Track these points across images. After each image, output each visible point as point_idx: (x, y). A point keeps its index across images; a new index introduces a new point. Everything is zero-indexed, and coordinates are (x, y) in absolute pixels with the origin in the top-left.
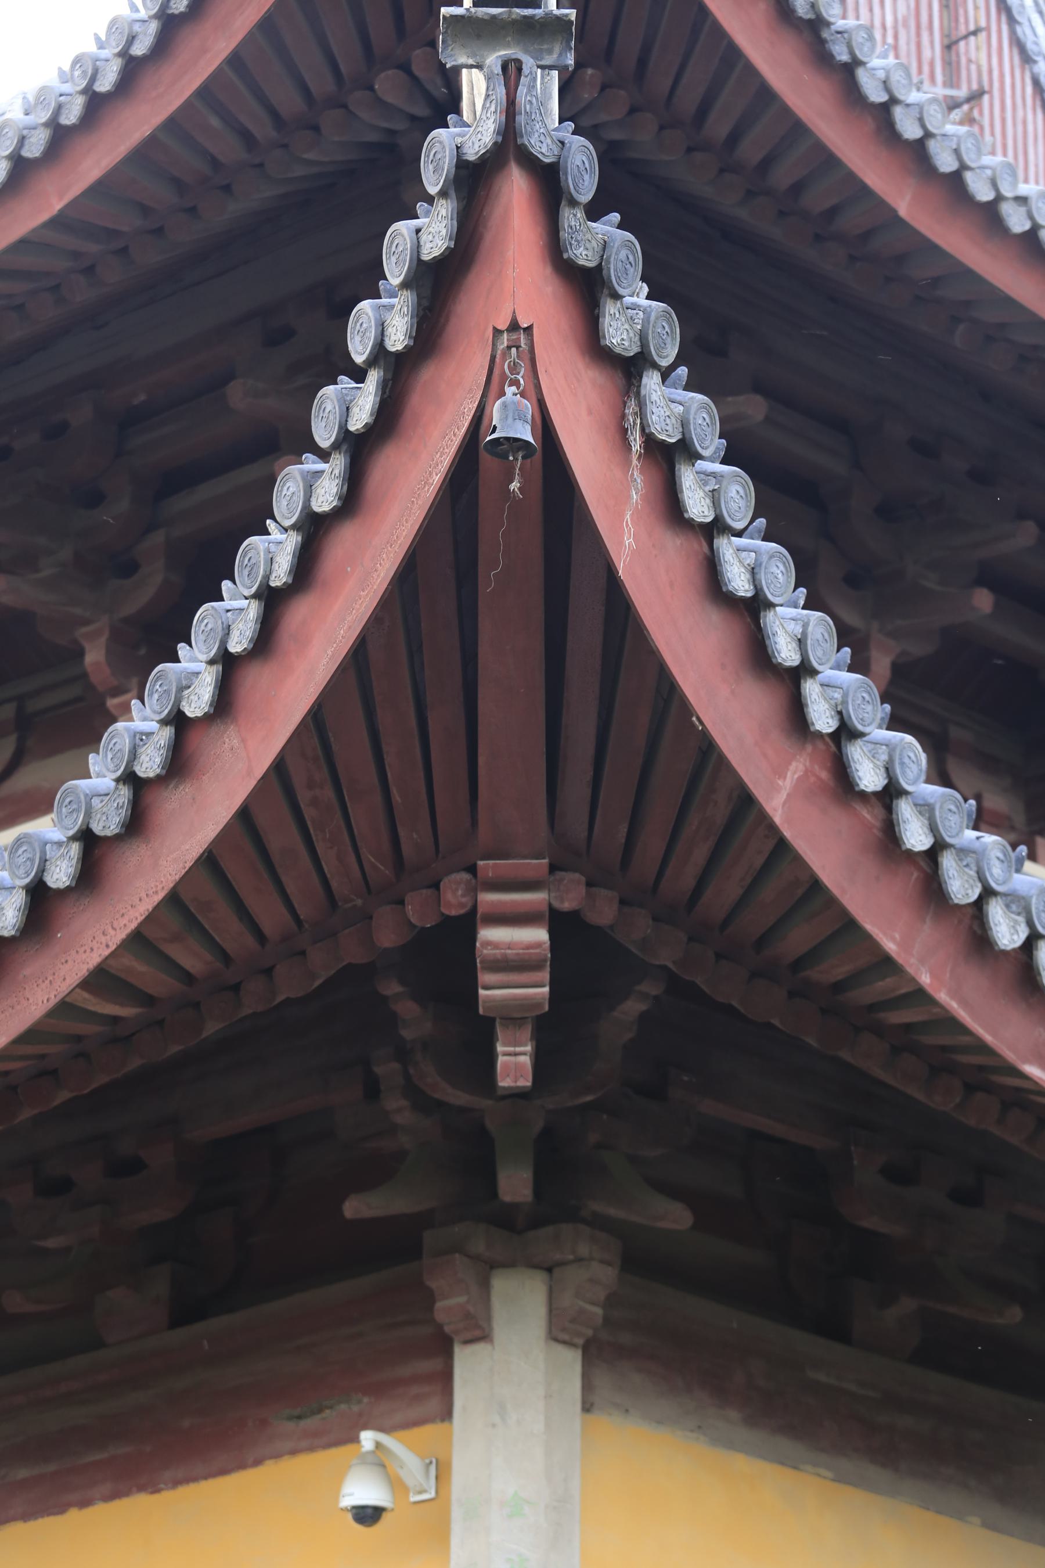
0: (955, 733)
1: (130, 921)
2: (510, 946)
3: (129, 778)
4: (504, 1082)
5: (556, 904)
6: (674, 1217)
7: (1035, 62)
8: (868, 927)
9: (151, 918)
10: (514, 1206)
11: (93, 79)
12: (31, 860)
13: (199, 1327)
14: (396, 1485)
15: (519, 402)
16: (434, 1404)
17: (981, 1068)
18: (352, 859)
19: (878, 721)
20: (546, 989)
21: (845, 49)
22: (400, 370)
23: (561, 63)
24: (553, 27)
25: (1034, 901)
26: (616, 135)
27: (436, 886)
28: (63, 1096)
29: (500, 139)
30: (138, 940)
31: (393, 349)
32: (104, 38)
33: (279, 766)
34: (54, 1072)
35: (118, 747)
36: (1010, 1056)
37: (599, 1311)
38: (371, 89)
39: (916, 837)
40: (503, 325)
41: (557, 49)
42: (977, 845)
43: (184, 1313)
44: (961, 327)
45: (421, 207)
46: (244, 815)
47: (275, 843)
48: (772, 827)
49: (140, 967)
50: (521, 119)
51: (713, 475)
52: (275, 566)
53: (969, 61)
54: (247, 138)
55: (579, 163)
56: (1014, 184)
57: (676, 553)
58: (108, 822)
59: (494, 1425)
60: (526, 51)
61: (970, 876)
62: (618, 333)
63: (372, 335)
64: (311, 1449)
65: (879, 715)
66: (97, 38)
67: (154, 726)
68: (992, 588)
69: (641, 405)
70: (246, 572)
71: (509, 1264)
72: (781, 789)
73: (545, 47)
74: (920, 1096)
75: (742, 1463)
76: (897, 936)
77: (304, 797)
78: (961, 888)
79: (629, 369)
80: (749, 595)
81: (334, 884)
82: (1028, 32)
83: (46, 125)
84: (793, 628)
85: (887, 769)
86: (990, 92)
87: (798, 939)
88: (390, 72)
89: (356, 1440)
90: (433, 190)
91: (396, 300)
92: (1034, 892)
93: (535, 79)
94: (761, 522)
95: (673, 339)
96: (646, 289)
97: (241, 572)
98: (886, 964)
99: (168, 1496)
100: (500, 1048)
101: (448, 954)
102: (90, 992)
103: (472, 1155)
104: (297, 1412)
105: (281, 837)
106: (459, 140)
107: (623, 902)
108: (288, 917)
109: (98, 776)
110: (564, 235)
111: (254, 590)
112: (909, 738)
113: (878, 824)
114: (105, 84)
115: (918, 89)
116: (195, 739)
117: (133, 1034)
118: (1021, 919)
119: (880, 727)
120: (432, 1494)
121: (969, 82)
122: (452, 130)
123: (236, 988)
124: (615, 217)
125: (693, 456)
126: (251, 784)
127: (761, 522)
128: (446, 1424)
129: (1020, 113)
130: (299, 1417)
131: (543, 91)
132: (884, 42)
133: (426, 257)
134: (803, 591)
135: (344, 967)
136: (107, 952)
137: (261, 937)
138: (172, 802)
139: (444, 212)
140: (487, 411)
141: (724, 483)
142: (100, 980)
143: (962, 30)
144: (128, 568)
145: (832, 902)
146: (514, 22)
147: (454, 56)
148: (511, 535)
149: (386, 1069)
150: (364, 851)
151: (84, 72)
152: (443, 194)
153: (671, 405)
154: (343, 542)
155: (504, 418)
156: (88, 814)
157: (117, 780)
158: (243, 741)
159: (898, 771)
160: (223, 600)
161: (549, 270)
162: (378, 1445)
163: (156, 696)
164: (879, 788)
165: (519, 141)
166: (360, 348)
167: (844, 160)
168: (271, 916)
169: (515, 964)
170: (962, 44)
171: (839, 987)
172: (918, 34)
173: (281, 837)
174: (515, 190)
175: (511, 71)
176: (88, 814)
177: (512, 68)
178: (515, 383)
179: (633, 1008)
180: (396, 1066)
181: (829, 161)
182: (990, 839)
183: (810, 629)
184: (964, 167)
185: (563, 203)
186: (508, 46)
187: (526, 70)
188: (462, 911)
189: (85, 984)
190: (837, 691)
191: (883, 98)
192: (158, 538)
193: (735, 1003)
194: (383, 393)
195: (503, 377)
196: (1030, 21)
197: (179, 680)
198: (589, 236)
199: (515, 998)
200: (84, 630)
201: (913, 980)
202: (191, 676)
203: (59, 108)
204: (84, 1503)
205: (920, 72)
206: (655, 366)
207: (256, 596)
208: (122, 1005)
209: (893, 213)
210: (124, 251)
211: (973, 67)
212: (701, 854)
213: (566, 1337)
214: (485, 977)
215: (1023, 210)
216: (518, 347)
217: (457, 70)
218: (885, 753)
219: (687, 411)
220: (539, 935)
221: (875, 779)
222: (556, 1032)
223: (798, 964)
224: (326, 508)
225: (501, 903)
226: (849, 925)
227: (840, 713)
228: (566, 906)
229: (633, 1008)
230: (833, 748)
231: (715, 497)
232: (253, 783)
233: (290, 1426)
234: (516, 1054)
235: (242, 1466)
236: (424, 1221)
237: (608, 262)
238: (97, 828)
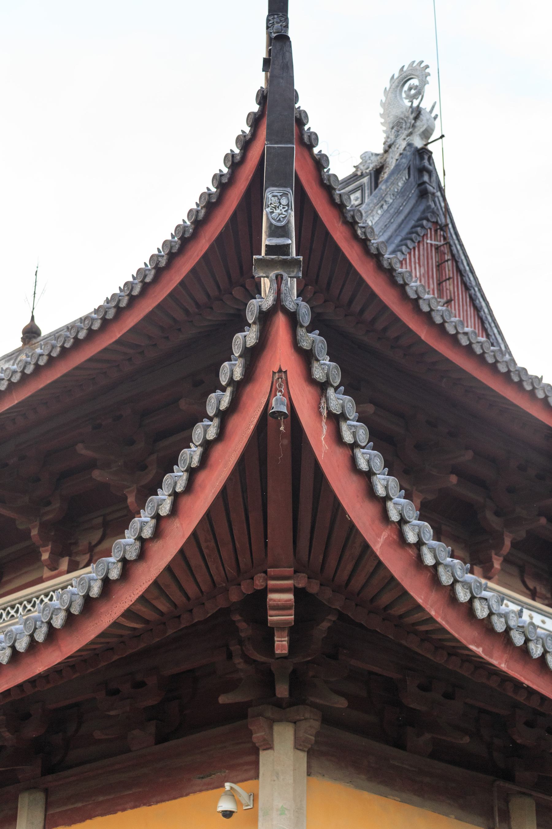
0: (444, 527)
1: (140, 592)
2: (279, 600)
3: (140, 538)
4: (278, 652)
5: (297, 585)
6: (341, 703)
7: (470, 290)
8: (412, 593)
9: (147, 590)
10: (282, 699)
11: (131, 291)
12: (104, 569)
13: (166, 744)
14: (238, 803)
15: (282, 398)
16: (252, 773)
17: (454, 647)
18: (221, 568)
19: (415, 517)
20: (293, 617)
21: (402, 279)
22: (239, 388)
23: (297, 276)
24: (294, 263)
25: (473, 584)
26: (319, 310)
27: (252, 578)
28: (116, 658)
29: (275, 303)
30: (142, 599)
31: (236, 380)
32: (135, 276)
33: (194, 534)
34: (112, 649)
35: (135, 527)
36: (464, 642)
37: (313, 738)
38: (231, 294)
39: (429, 560)
40: (276, 371)
41: (296, 271)
42: (452, 563)
43: (161, 739)
44: (444, 380)
45: (246, 328)
46: (182, 552)
47: (193, 563)
48: (376, 557)
49: (144, 609)
50: (283, 296)
51: (354, 426)
52: (193, 460)
53: (447, 289)
54: (187, 312)
55: (303, 311)
56: (463, 328)
57: (340, 455)
58: (132, 555)
59: (274, 781)
60: (285, 272)
61: (449, 575)
62: (318, 374)
63: (228, 374)
64: (207, 790)
65: (415, 515)
66: (133, 276)
67: (149, 519)
68: (457, 475)
69: (327, 400)
70: (182, 462)
71: (280, 721)
72: (379, 542)
73: (291, 270)
74: (432, 658)
75: (366, 795)
76: (422, 597)
77: (203, 545)
78: (446, 579)
79: (322, 387)
80: (367, 470)
81: (215, 578)
82: (468, 279)
83: (114, 307)
84: (383, 482)
85: (418, 535)
86: (454, 300)
87: (385, 599)
88: (238, 288)
89: (223, 786)
90: (250, 322)
91: (237, 362)
92: (472, 581)
93: (287, 281)
94: (371, 444)
95: (339, 376)
96: (329, 358)
97: (180, 462)
98: (419, 608)
99: (154, 807)
100: (276, 639)
101: (258, 601)
102: (125, 618)
103: (267, 680)
104: (202, 776)
105: (196, 561)
106: (260, 303)
107: (321, 585)
108: (198, 590)
109: (128, 538)
110: (298, 338)
111: (185, 468)
112: (426, 524)
113: (415, 556)
114: (136, 292)
115: (428, 294)
116: (163, 524)
117: (141, 634)
118: (468, 591)
119: (415, 519)
120: (252, 807)
121: (447, 296)
122: (257, 300)
123: (179, 617)
124: (317, 332)
125: (346, 419)
126: (184, 540)
127: (371, 444)
128: (257, 780)
129: (465, 308)
130: (202, 778)
131: (291, 286)
132: (416, 276)
133: (248, 346)
134: (387, 469)
135: (219, 610)
136: (131, 603)
137: (188, 598)
138: (155, 548)
139: (254, 330)
140: (270, 402)
141: (358, 429)
142: (129, 614)
143: (444, 278)
144: (144, 468)
145: (399, 584)
146: (280, 261)
147: (258, 273)
148: (279, 447)
149: (235, 648)
150: (226, 566)
151: (128, 288)
152: (254, 323)
153: (337, 400)
154: (218, 450)
155: (276, 404)
156: (125, 552)
157: (135, 539)
158: (181, 524)
159: (422, 535)
160: (174, 472)
161: (293, 350)
162: (231, 788)
163: (149, 508)
164: (415, 542)
165: (282, 304)
166: (224, 380)
167: (402, 319)
168: (192, 590)
169: (281, 607)
170: (444, 283)
171: (401, 617)
172: (428, 280)
173: (196, 561)
174: (280, 322)
175: (279, 279)
176: (125, 552)
177: (279, 277)
178: (281, 391)
179: (325, 625)
180: (238, 647)
181: (396, 319)
182: (456, 561)
183: (389, 483)
184: (444, 322)
185: (298, 326)
186: (278, 270)
187: (284, 278)
188: (262, 588)
189: (123, 615)
190: (399, 506)
191: (416, 297)
192: (154, 457)
193: (362, 622)
194: (233, 396)
195: (276, 389)
196: (468, 275)
197: (158, 502)
198: (307, 338)
199: (281, 620)
200: (127, 490)
201: (428, 614)
202: (162, 501)
203: (119, 301)
204: (124, 810)
205: (429, 287)
206: (332, 386)
207: (186, 471)
208: (137, 623)
209: (420, 338)
210: (142, 353)
211: (448, 291)
212: (350, 567)
213: (301, 748)
214: (270, 612)
215: (466, 337)
216: (282, 378)
217: (260, 278)
218: (416, 529)
219: (344, 402)
220: (290, 596)
221: (414, 538)
222: (296, 632)
223: (386, 608)
224: (212, 438)
225: (276, 585)
226: (405, 593)
227: (401, 514)
228: (300, 586)
229: (325, 625)
230: (398, 527)
231: (354, 434)
232: (185, 540)
233: (199, 781)
234: (282, 641)
235: (182, 796)
236: (249, 704)
237: (315, 348)
238: (128, 557)
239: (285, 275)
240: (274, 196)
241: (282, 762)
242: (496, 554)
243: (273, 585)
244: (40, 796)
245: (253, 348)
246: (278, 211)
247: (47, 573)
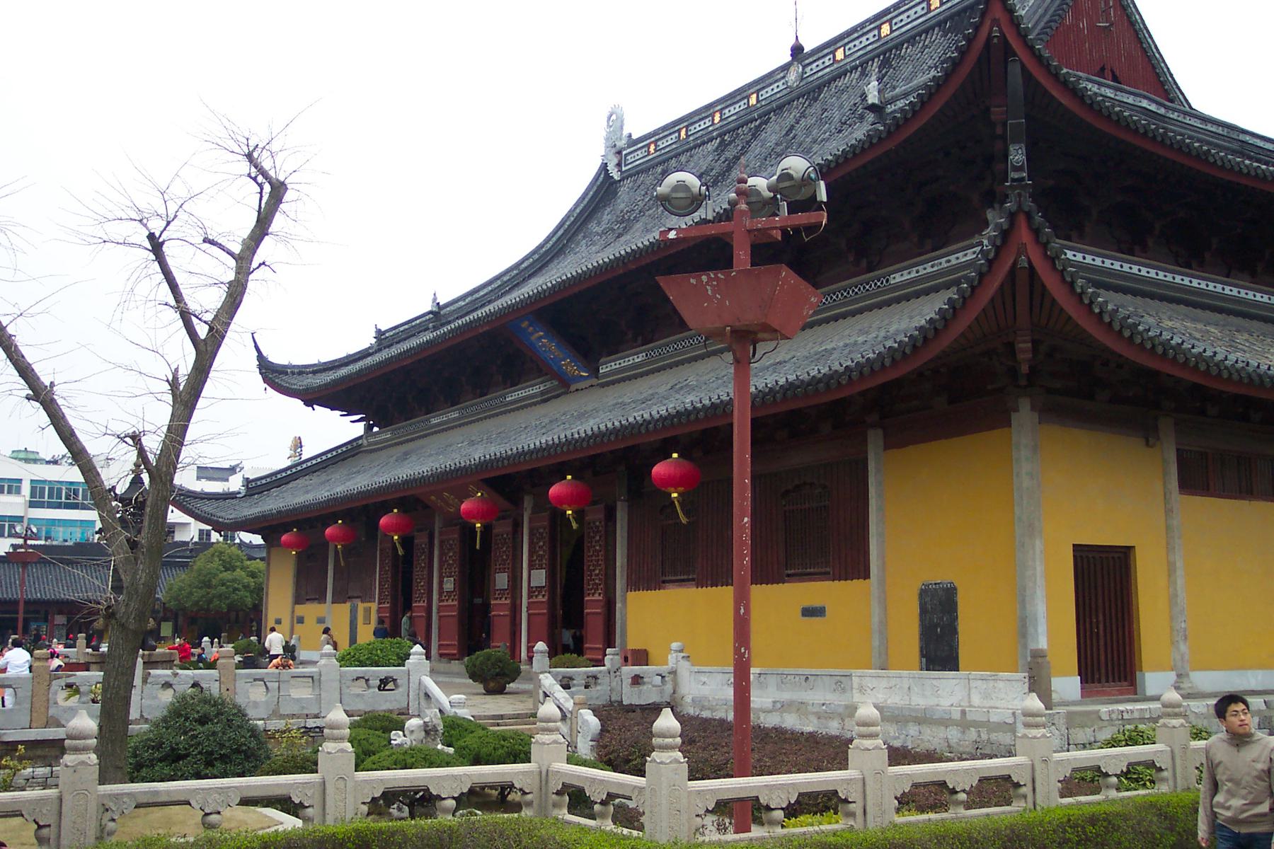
101: (1011, 347)
128: (1006, 429)
174: (1021, 219)
175: (1020, 195)
220: (1030, 345)
241: (1024, 416)
244: (880, 432)
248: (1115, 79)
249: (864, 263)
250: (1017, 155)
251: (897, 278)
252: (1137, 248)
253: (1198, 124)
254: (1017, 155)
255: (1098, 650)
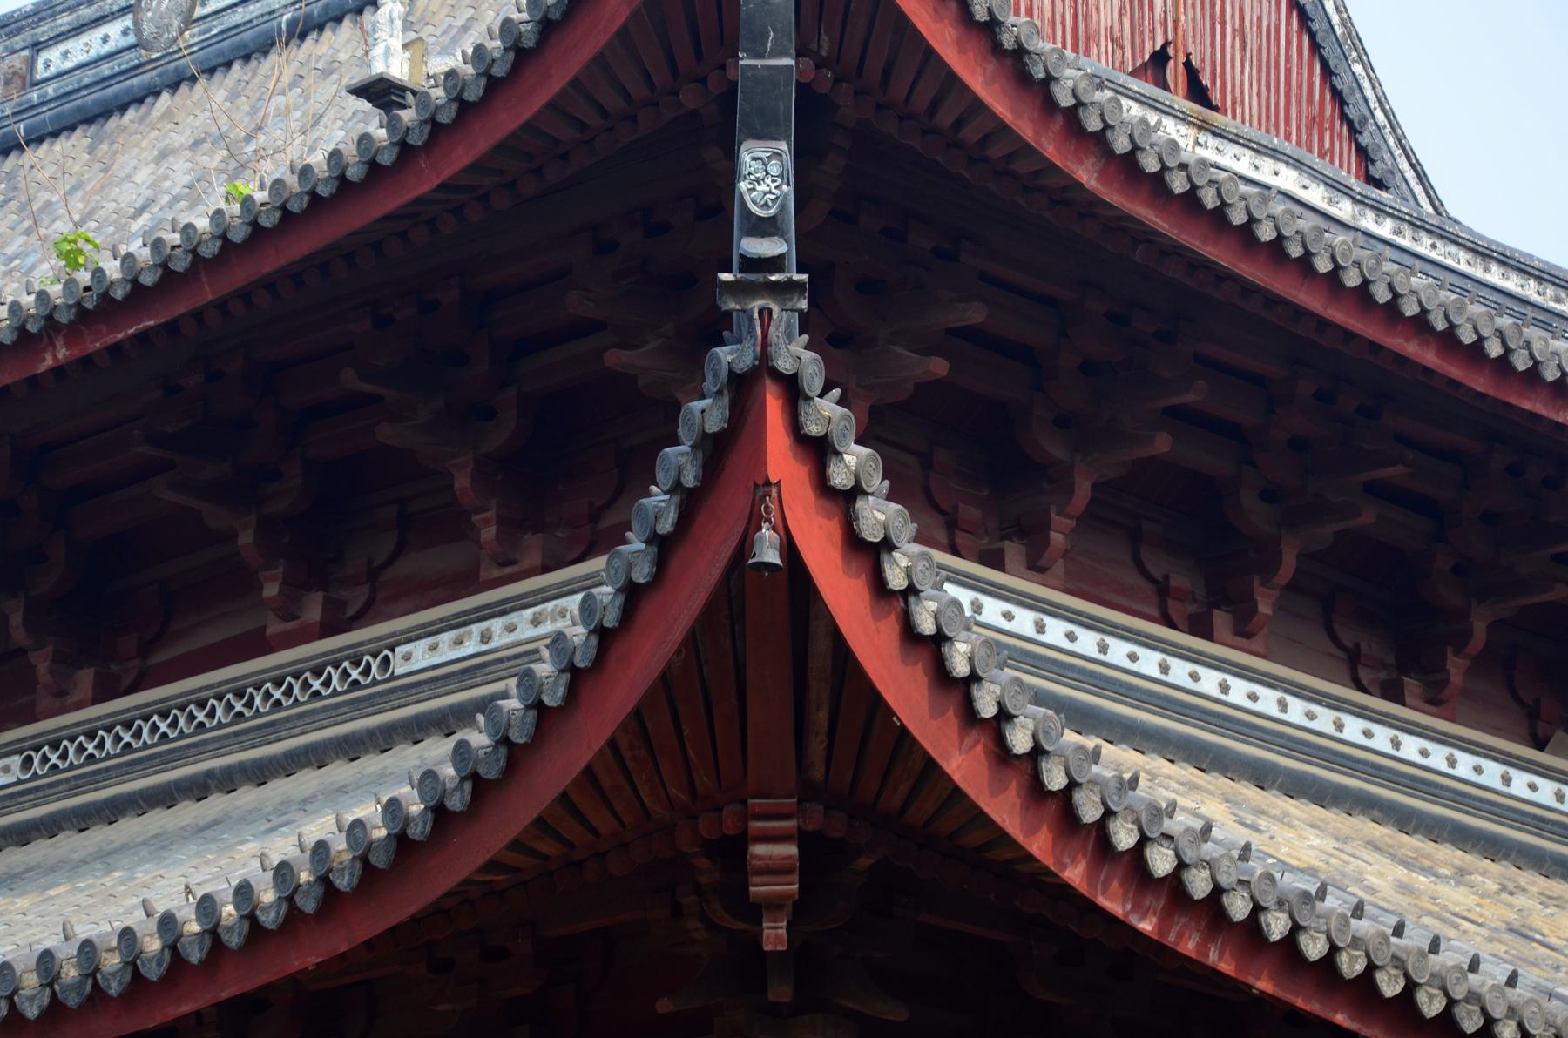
2: (770, 858)
21: (1041, 68)
40: (760, 482)
50: (772, 349)
60: (775, 300)
62: (840, 477)
63: (673, 473)
77: (627, 754)
101: (732, 851)
169: (775, 870)
178: (768, 520)
186: (762, 297)
187: (775, 316)
200: (455, 461)
212: (904, 789)
215: (1184, 173)
220: (791, 850)
222: (800, 911)
239: (775, 309)
240: (754, 159)
242: (1262, 584)
243: (759, 829)
245: (717, 436)
246: (763, 188)
247: (274, 627)
248: (1198, 93)
249: (313, 611)
250: (764, 176)
251: (418, 657)
252: (1221, 619)
253: (1461, 261)
254: (764, 176)
255: (1300, 86)
